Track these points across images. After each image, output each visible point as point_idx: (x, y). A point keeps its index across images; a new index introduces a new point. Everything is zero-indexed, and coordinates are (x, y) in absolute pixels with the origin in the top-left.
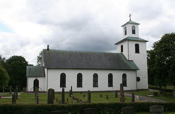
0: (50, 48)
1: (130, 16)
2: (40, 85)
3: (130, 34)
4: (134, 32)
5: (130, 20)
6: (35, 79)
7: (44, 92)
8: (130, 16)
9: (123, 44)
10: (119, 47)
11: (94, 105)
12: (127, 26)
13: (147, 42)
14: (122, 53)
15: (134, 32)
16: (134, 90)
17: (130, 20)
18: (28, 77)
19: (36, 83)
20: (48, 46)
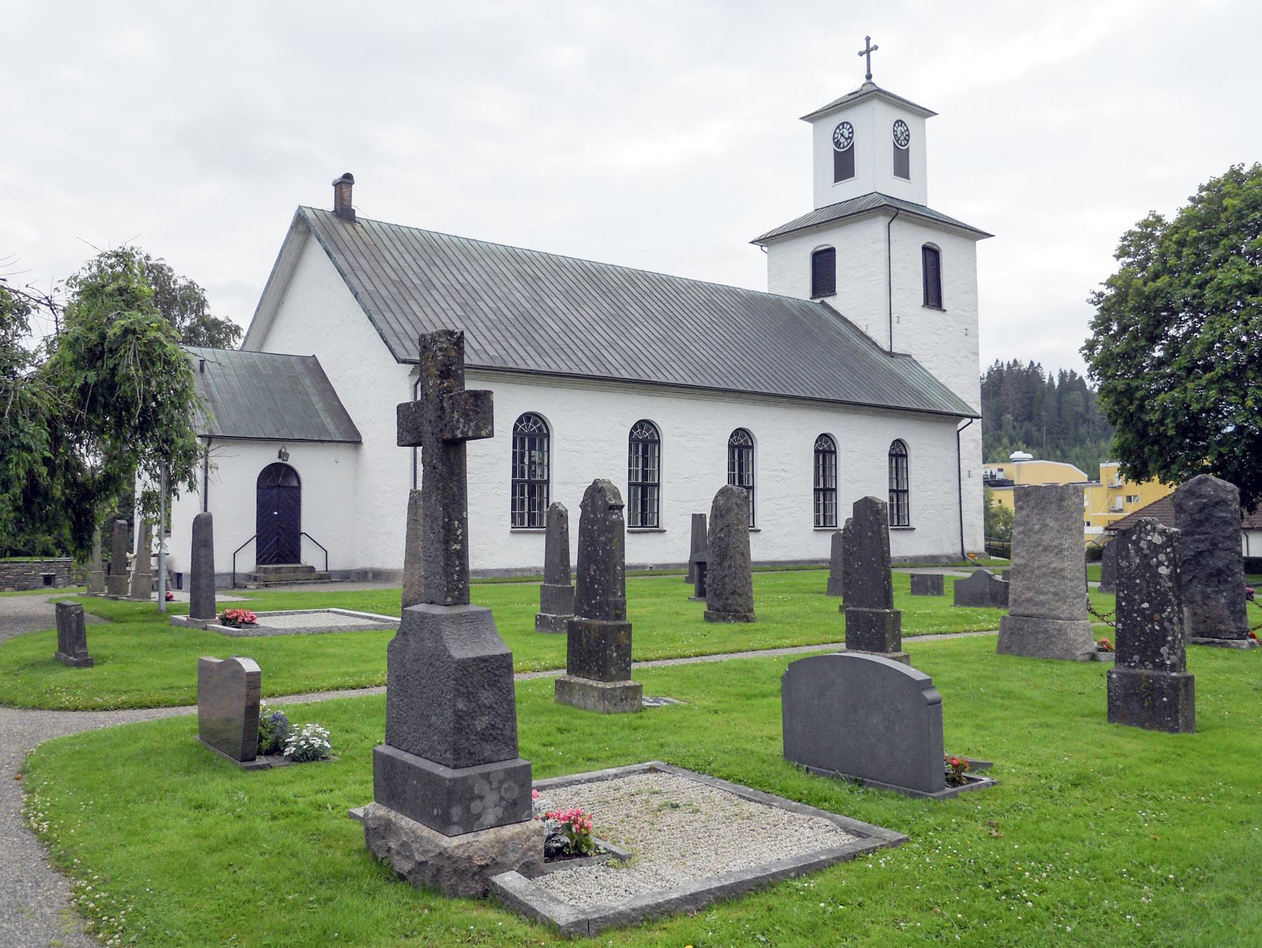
0: (364, 205)
1: (868, 51)
2: (316, 517)
3: (874, 175)
4: (902, 167)
5: (869, 77)
6: (269, 456)
7: (377, 576)
8: (868, 51)
9: (841, 241)
10: (799, 258)
11: (888, 577)
12: (856, 117)
13: (980, 243)
14: (828, 300)
15: (902, 167)
16: (948, 557)
17: (869, 77)
18: (209, 439)
19: (279, 494)
20: (345, 183)
